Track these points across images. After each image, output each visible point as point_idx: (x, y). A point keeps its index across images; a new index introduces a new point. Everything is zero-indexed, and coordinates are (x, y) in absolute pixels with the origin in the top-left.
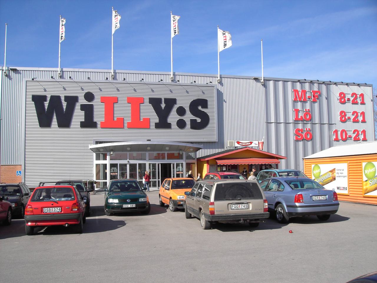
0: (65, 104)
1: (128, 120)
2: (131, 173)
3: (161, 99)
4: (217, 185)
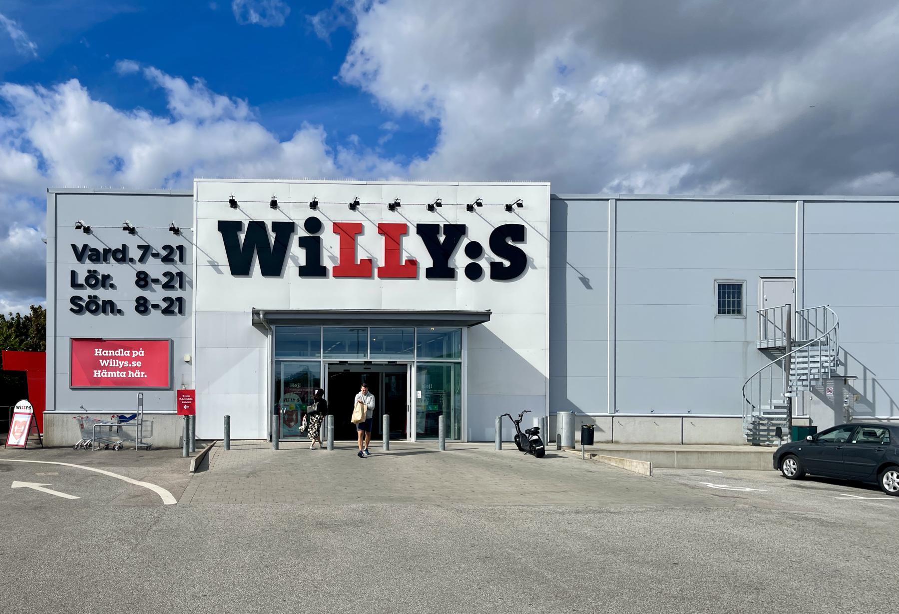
0: (272, 236)
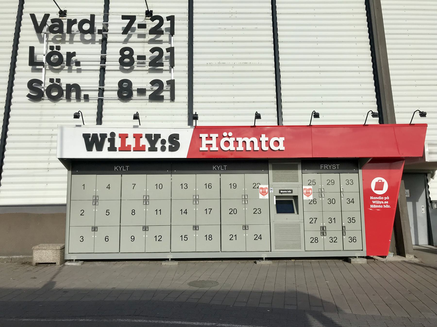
1: (133, 145)
2: (30, 256)
3: (152, 134)
4: (292, 200)
